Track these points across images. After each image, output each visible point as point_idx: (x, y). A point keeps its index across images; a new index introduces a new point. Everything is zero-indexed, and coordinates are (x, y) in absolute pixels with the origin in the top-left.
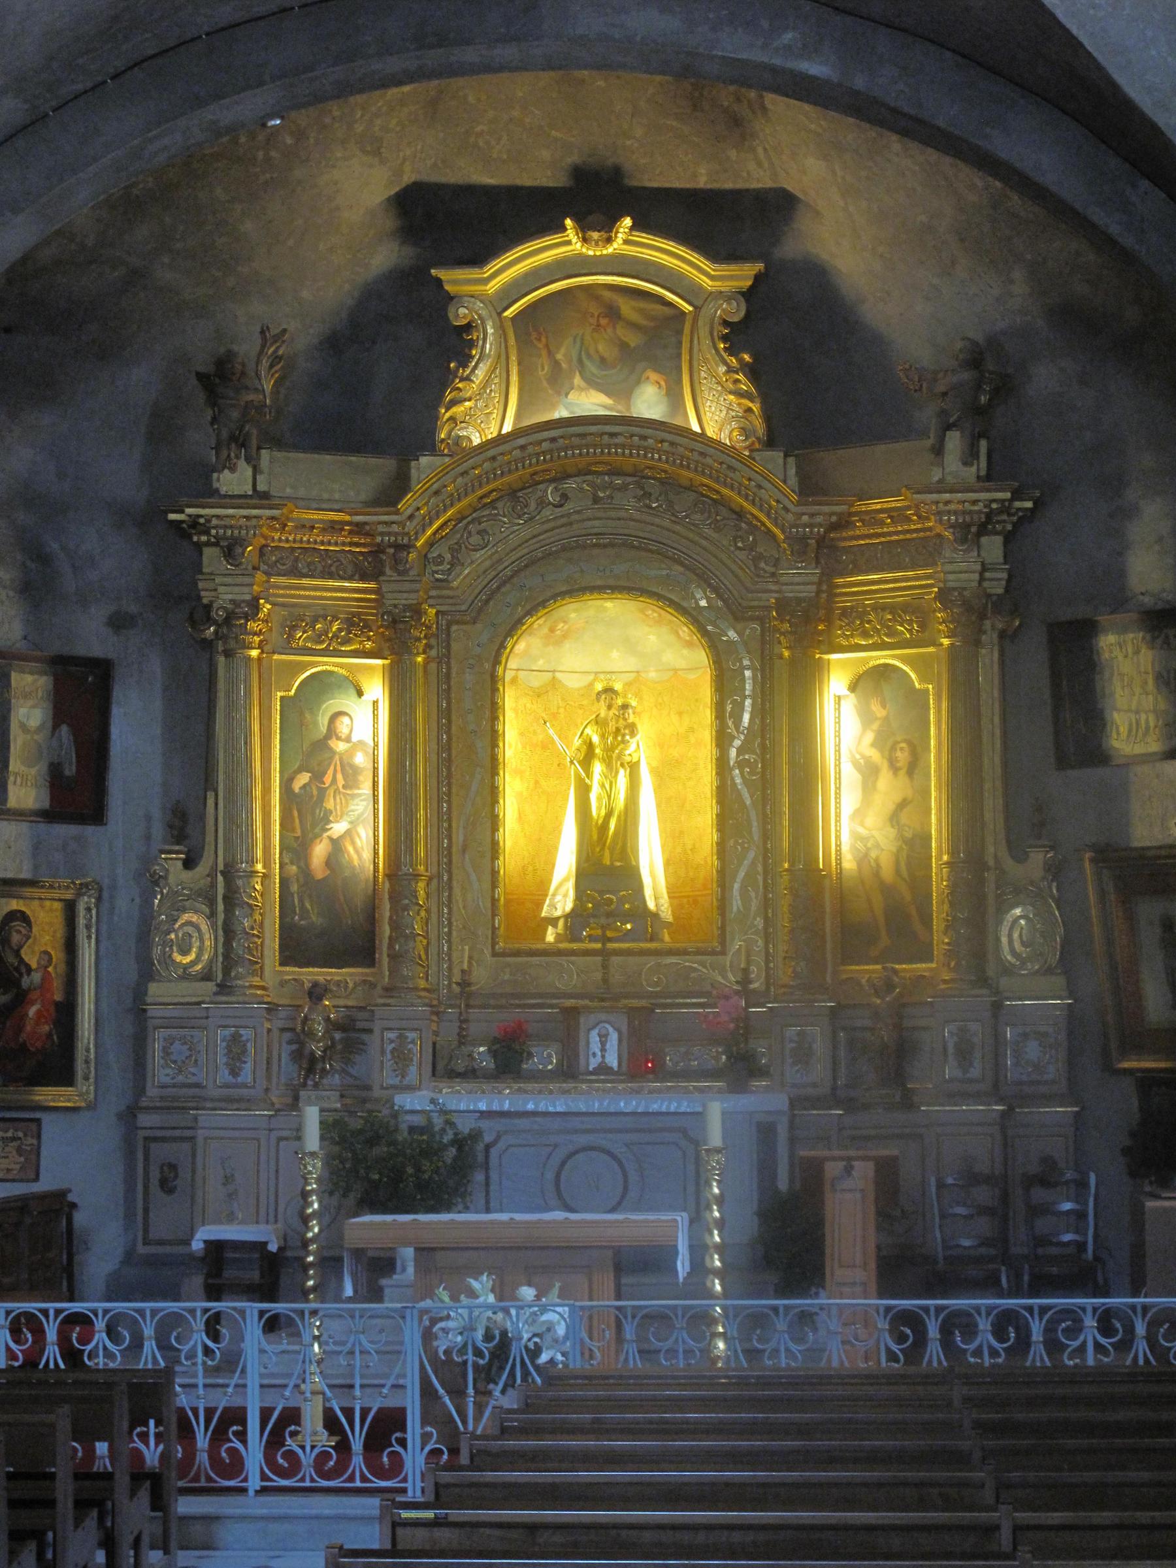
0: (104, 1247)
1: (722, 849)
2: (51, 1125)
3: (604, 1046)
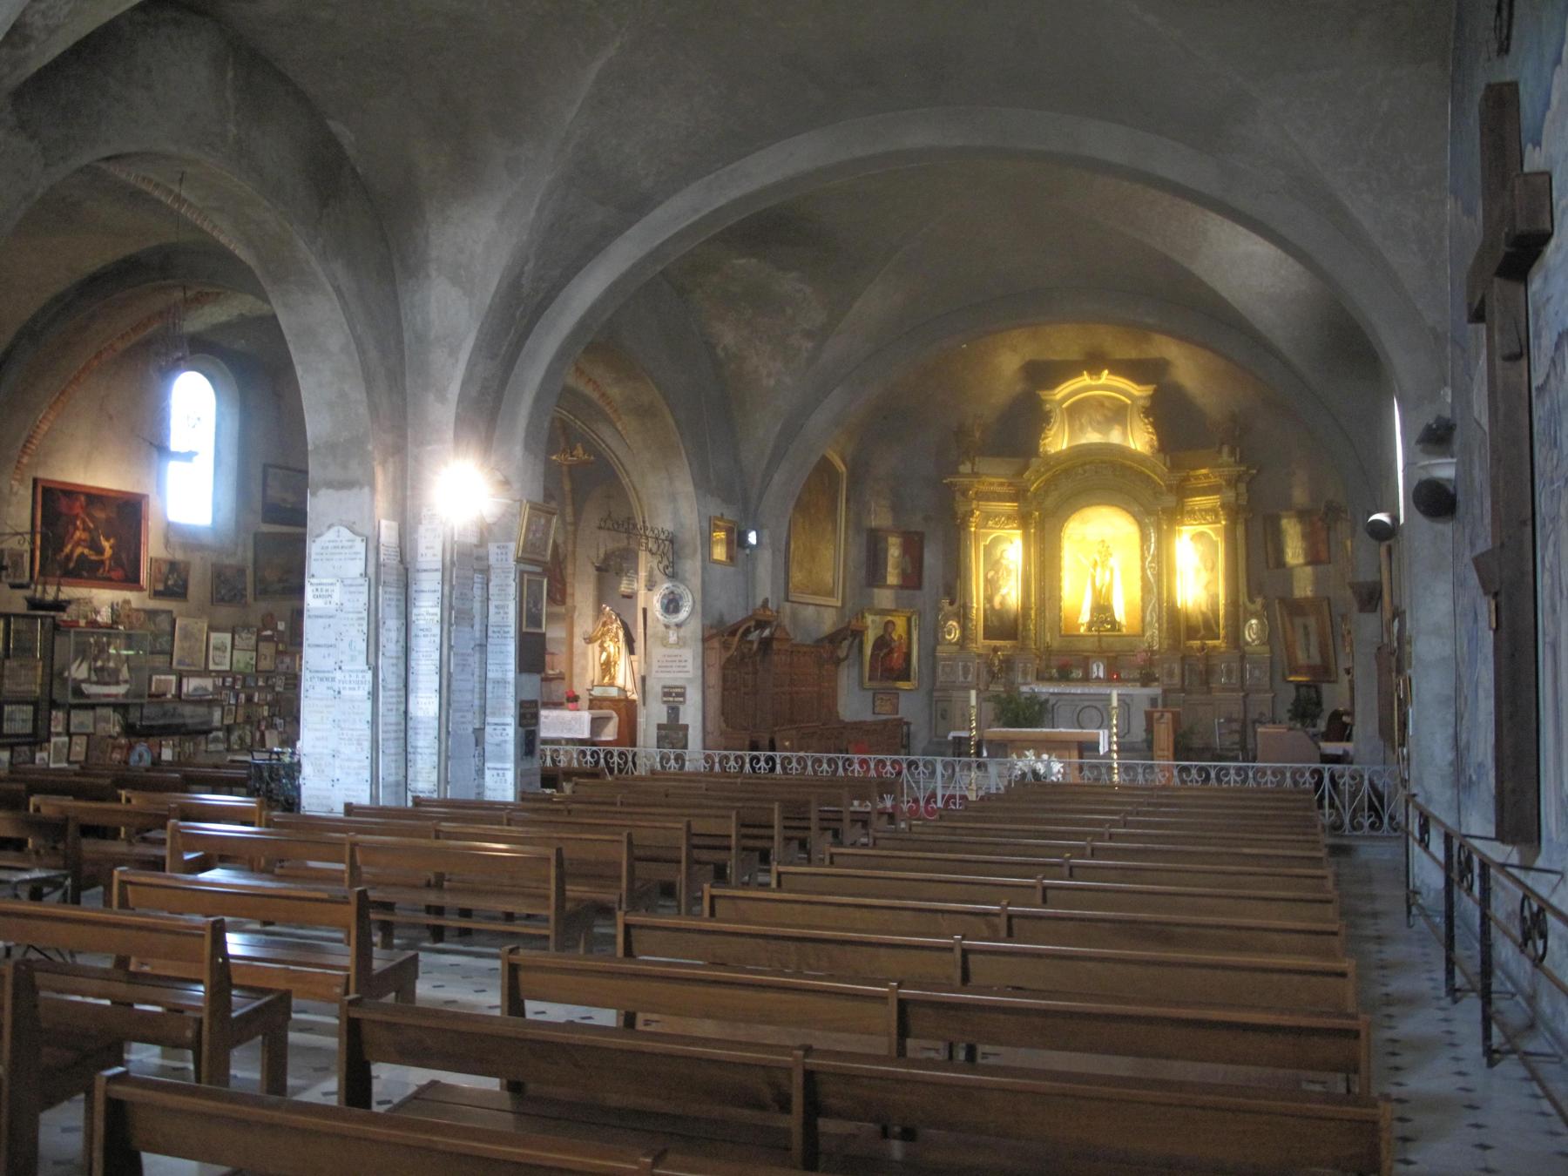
0: (921, 738)
1: (1143, 599)
2: (903, 698)
3: (1099, 670)
